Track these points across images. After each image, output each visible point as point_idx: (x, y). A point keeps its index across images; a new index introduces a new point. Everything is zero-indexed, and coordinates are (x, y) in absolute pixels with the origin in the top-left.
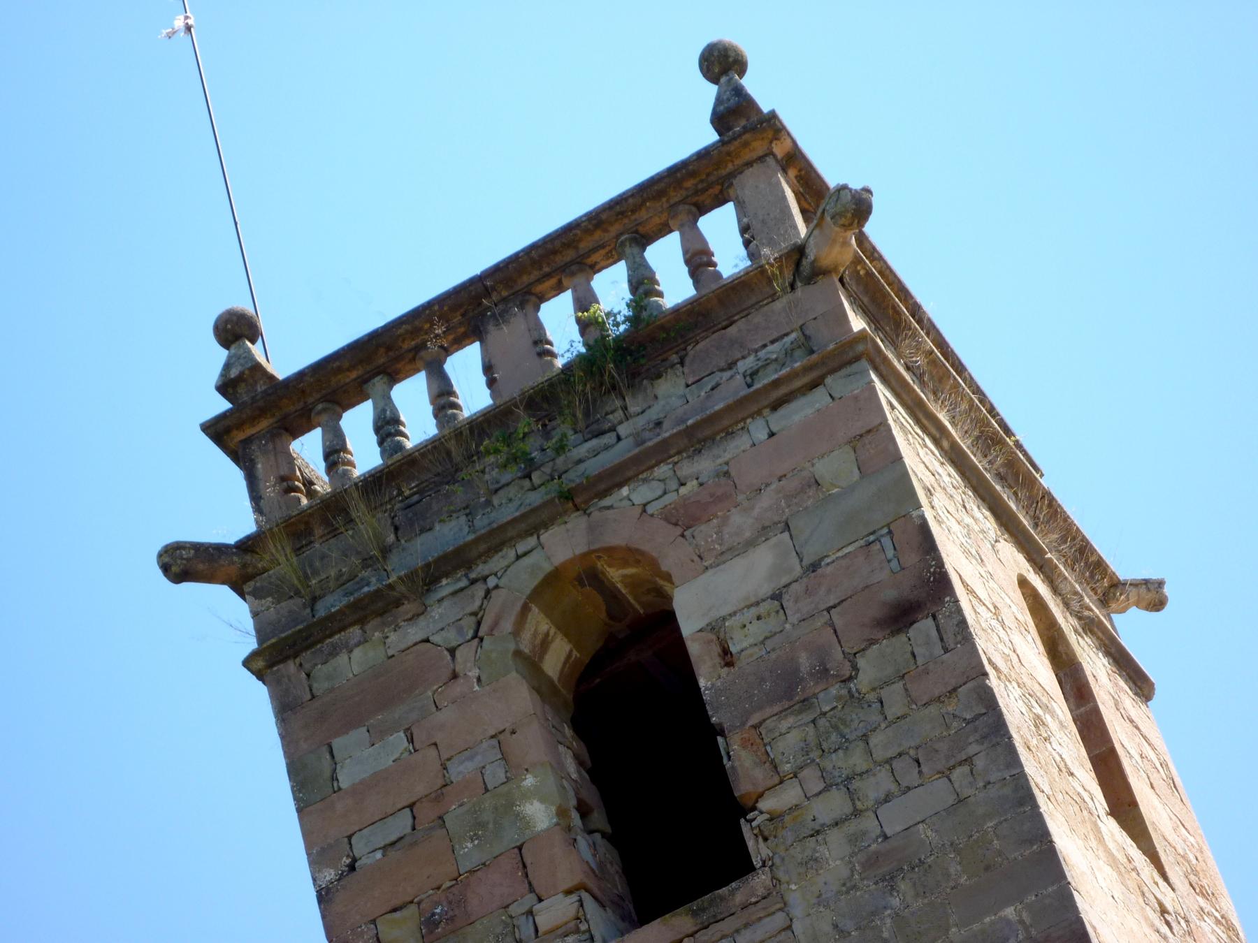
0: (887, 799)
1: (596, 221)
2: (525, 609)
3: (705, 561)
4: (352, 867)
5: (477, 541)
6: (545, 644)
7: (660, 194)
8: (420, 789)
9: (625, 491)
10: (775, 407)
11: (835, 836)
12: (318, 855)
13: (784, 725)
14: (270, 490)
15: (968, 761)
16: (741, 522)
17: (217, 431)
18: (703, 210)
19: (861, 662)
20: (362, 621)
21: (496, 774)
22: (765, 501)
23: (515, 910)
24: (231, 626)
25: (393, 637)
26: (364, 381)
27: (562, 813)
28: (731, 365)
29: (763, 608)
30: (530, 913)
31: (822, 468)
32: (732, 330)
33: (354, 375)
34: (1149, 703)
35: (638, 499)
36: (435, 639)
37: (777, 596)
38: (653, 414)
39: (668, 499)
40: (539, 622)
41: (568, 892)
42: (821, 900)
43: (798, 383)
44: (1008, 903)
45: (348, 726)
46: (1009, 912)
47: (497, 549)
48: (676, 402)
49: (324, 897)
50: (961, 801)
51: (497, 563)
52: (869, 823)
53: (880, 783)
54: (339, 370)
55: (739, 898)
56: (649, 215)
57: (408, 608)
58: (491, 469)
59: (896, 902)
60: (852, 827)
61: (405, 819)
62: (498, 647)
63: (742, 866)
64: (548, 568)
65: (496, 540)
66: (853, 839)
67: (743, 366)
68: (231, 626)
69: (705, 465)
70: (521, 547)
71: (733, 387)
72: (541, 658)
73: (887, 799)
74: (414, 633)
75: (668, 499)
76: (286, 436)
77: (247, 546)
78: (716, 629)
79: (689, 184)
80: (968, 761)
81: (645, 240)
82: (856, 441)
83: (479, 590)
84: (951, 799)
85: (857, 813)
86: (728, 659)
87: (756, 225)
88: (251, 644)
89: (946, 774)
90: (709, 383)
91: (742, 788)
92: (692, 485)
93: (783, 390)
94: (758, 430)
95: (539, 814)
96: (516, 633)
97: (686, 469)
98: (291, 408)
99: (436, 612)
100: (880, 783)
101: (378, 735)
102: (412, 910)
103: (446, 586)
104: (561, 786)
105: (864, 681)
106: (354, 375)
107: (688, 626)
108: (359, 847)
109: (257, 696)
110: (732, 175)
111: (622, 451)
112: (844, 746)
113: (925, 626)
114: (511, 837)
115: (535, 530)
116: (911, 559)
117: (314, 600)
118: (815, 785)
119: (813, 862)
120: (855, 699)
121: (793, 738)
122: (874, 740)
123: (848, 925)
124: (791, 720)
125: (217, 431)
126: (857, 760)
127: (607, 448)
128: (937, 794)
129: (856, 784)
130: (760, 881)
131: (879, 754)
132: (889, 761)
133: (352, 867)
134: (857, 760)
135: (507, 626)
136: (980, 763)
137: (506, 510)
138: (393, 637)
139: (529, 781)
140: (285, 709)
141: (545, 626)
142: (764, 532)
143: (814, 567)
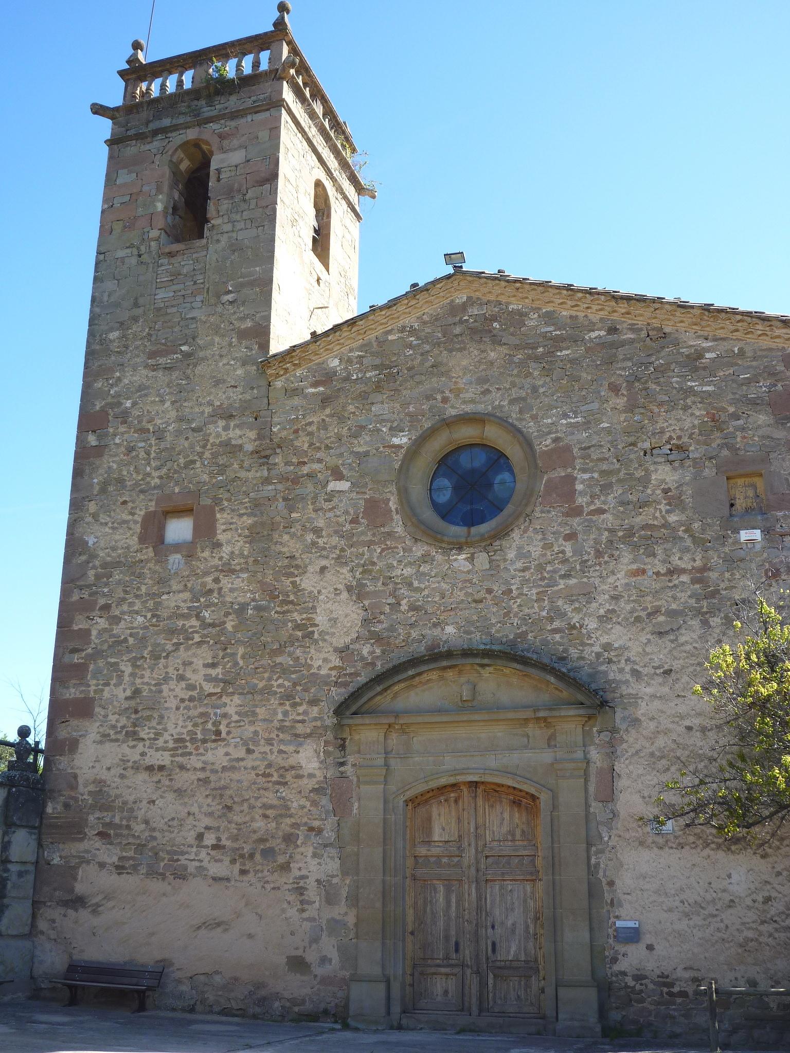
0: (241, 230)
1: (232, 44)
2: (176, 150)
3: (223, 150)
4: (112, 206)
5: (170, 127)
6: (181, 161)
7: (251, 42)
8: (135, 191)
9: (211, 124)
10: (256, 113)
11: (226, 235)
12: (105, 200)
13: (225, 202)
14: (128, 97)
15: (263, 226)
16: (236, 142)
17: (122, 74)
18: (263, 50)
19: (249, 191)
20: (137, 140)
21: (153, 192)
22: (244, 139)
23: (145, 230)
24: (732, 505)
25: (142, 146)
26: (162, 71)
27: (166, 208)
28: (250, 98)
29: (231, 169)
30: (148, 232)
31: (260, 134)
32: (254, 87)
33: (160, 69)
34: (105, 127)
35: (214, 127)
36: (152, 151)
37: (236, 166)
38: (226, 105)
39: (221, 130)
40: (180, 154)
41: (159, 229)
42: (216, 252)
43: (264, 108)
44: (257, 266)
45: (123, 168)
46: (257, 269)
47: (175, 130)
48: (233, 103)
49: (103, 212)
50: (258, 236)
51: (174, 134)
52: (234, 235)
53: (242, 225)
54: (156, 67)
55: (197, 244)
56: (248, 46)
57: (149, 139)
58: (183, 107)
59: (233, 257)
60: (230, 234)
61: (128, 198)
62: (166, 158)
63: (201, 236)
64: (185, 140)
65: (175, 128)
66: (230, 238)
67: (254, 98)
68: (732, 505)
69: (233, 124)
70: (181, 132)
71: (249, 103)
72: (180, 164)
73: (241, 230)
74: (148, 147)
75: (221, 130)
76: (139, 81)
77: (116, 109)
78: (219, 171)
79: (260, 41)
80: (263, 226)
81: (244, 54)
82: (271, 129)
83: (167, 140)
84: (256, 235)
85: (233, 231)
86: (219, 180)
87: (272, 59)
88: (109, 138)
89: (257, 227)
90: (243, 100)
91: (208, 216)
92: (228, 128)
93: (259, 109)
94: (249, 118)
95: (160, 206)
96: (172, 156)
97: (228, 123)
98: (142, 73)
99: (155, 143)
100: (242, 225)
101: (130, 172)
102: (121, 222)
103: (160, 136)
104: (664, 772)
105: (247, 197)
106: (160, 69)
107: (214, 166)
108: (115, 202)
109: (106, 148)
110: (272, 42)
111: (215, 113)
112: (237, 212)
113: (267, 186)
114: (151, 211)
115: (187, 128)
116: (272, 167)
117: (127, 130)
118: (226, 221)
119: (218, 241)
120: (245, 201)
121: (225, 206)
122: (244, 213)
123: (220, 260)
124: (227, 201)
125: (122, 74)
126: (238, 217)
127: (211, 110)
128: (253, 232)
129: (236, 223)
130: (204, 241)
131: (244, 217)
132: (246, 220)
133: (112, 206)
134: (238, 217)
135: (170, 153)
136: (266, 227)
137: (181, 120)
138: (142, 146)
139: (160, 197)
140: (111, 157)
141: (182, 156)
142: (240, 147)
143: (248, 161)
